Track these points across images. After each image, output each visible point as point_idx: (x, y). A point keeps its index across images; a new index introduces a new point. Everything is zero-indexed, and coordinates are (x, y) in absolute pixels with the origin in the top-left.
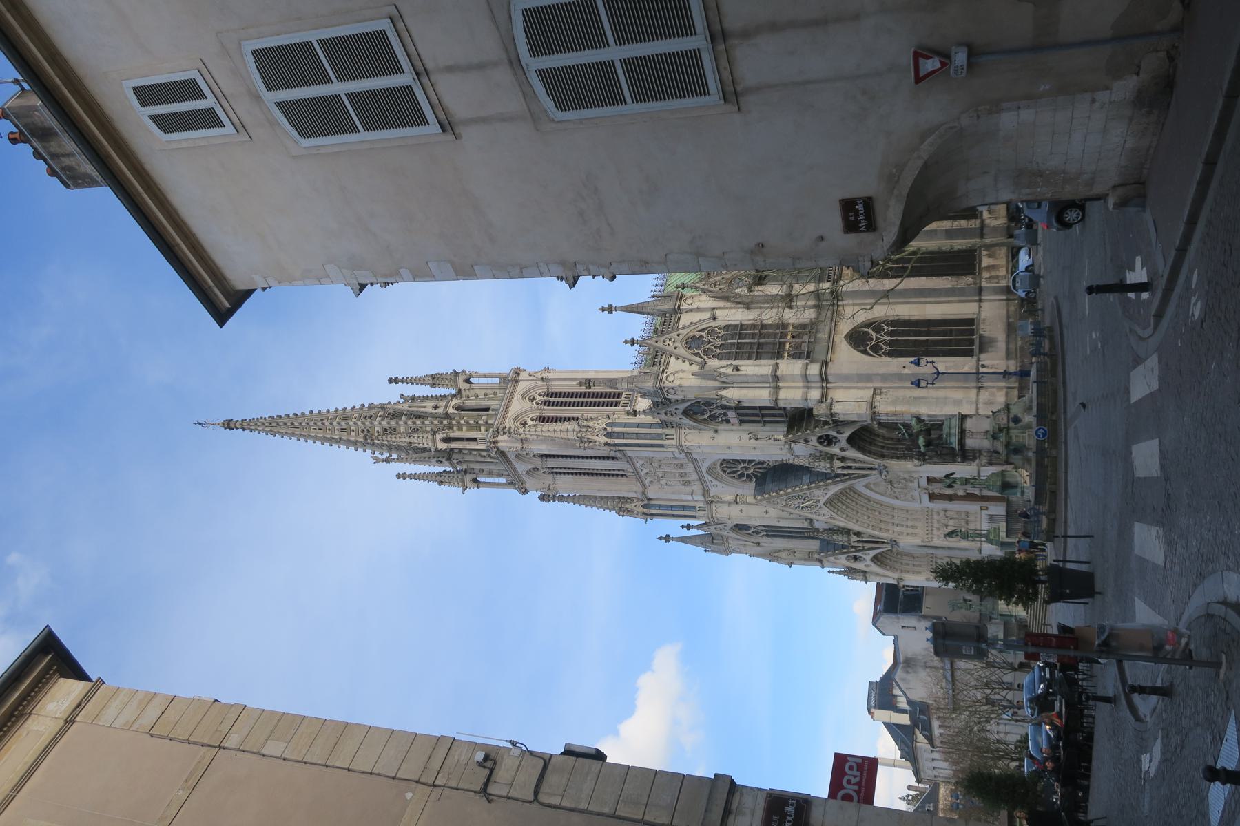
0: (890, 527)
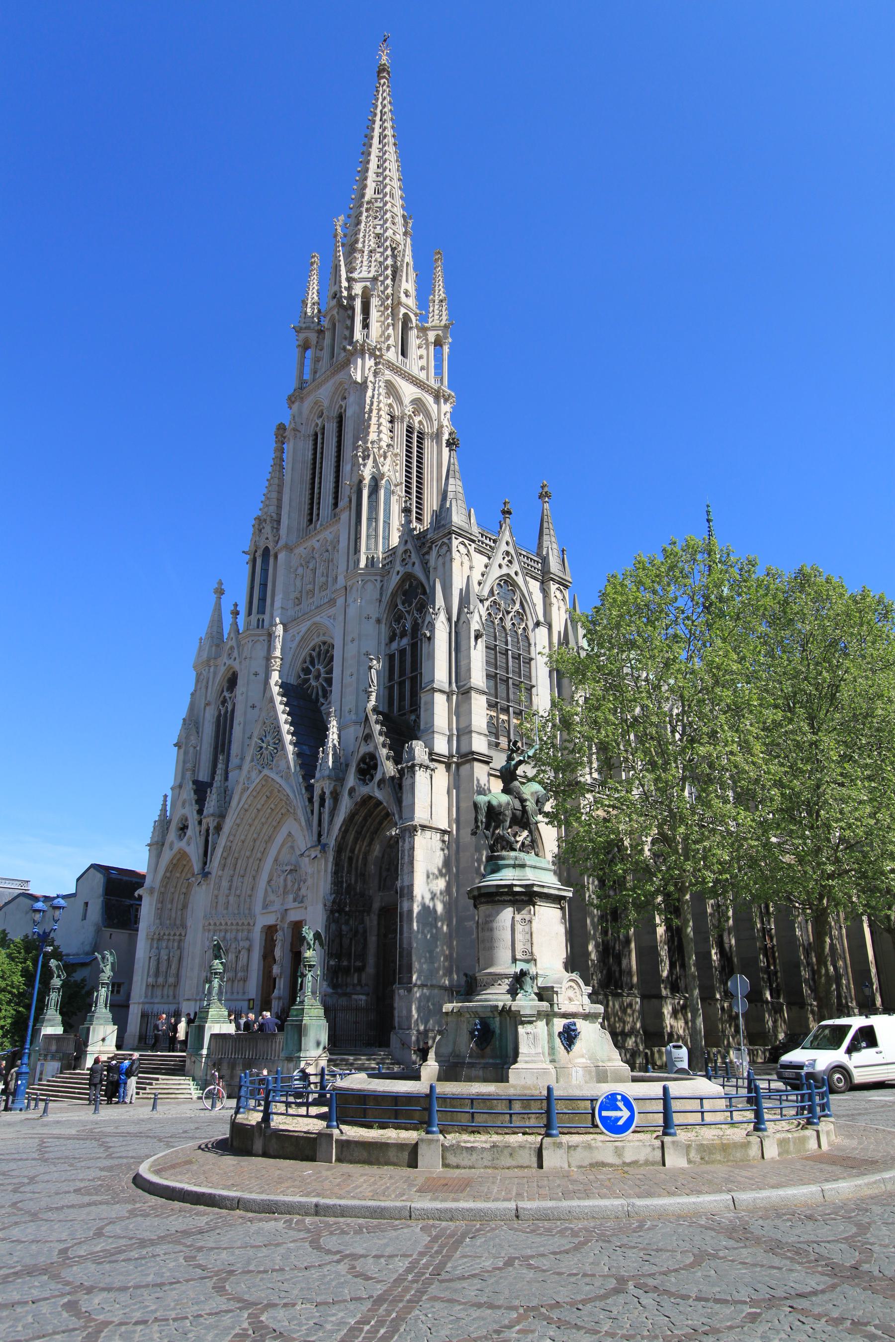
0: (228, 872)
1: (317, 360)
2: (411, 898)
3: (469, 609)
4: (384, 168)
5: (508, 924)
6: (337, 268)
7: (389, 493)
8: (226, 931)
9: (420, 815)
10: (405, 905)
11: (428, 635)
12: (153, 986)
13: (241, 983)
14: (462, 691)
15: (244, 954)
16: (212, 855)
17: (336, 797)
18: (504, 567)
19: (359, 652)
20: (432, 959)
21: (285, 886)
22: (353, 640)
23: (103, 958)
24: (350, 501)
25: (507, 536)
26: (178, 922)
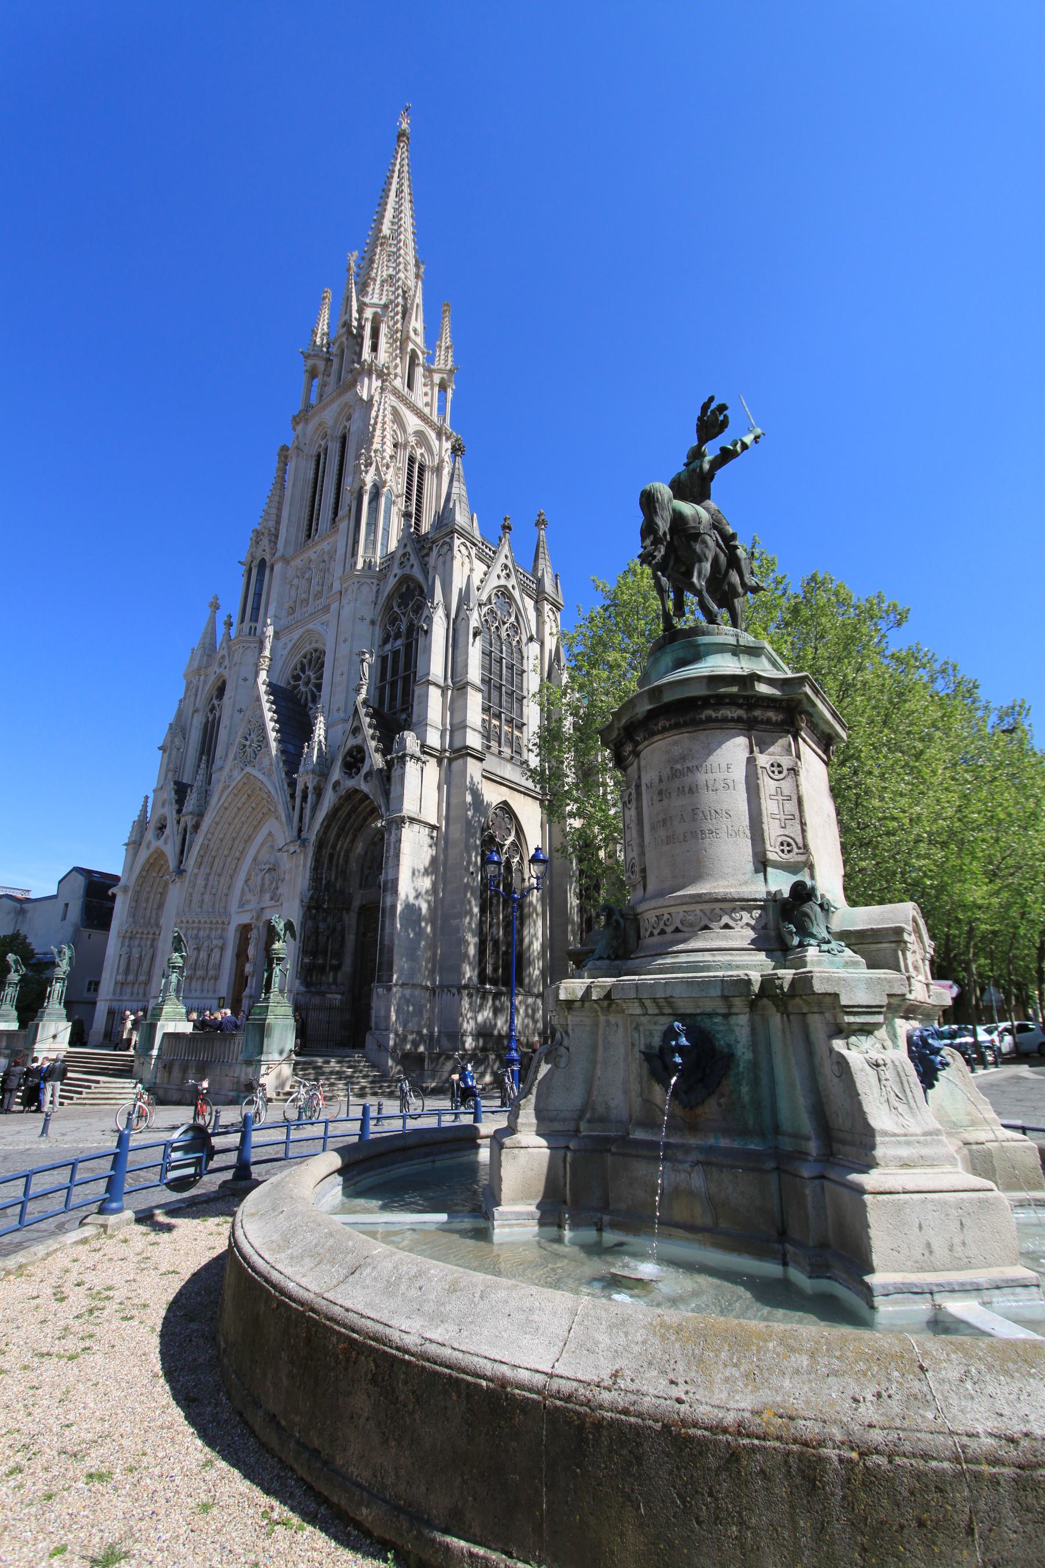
0: (204, 870)
1: (324, 385)
2: (395, 891)
3: (468, 605)
4: (399, 216)
5: (739, 773)
6: (349, 299)
7: (390, 503)
8: (199, 929)
9: (409, 807)
10: (389, 900)
11: (426, 628)
12: (122, 984)
13: (212, 981)
14: (458, 686)
15: (216, 954)
16: (188, 852)
17: (319, 792)
18: (502, 578)
19: (351, 652)
20: (412, 957)
21: (263, 885)
22: (345, 641)
23: (60, 952)
24: (350, 510)
25: (506, 550)
26: (153, 921)
